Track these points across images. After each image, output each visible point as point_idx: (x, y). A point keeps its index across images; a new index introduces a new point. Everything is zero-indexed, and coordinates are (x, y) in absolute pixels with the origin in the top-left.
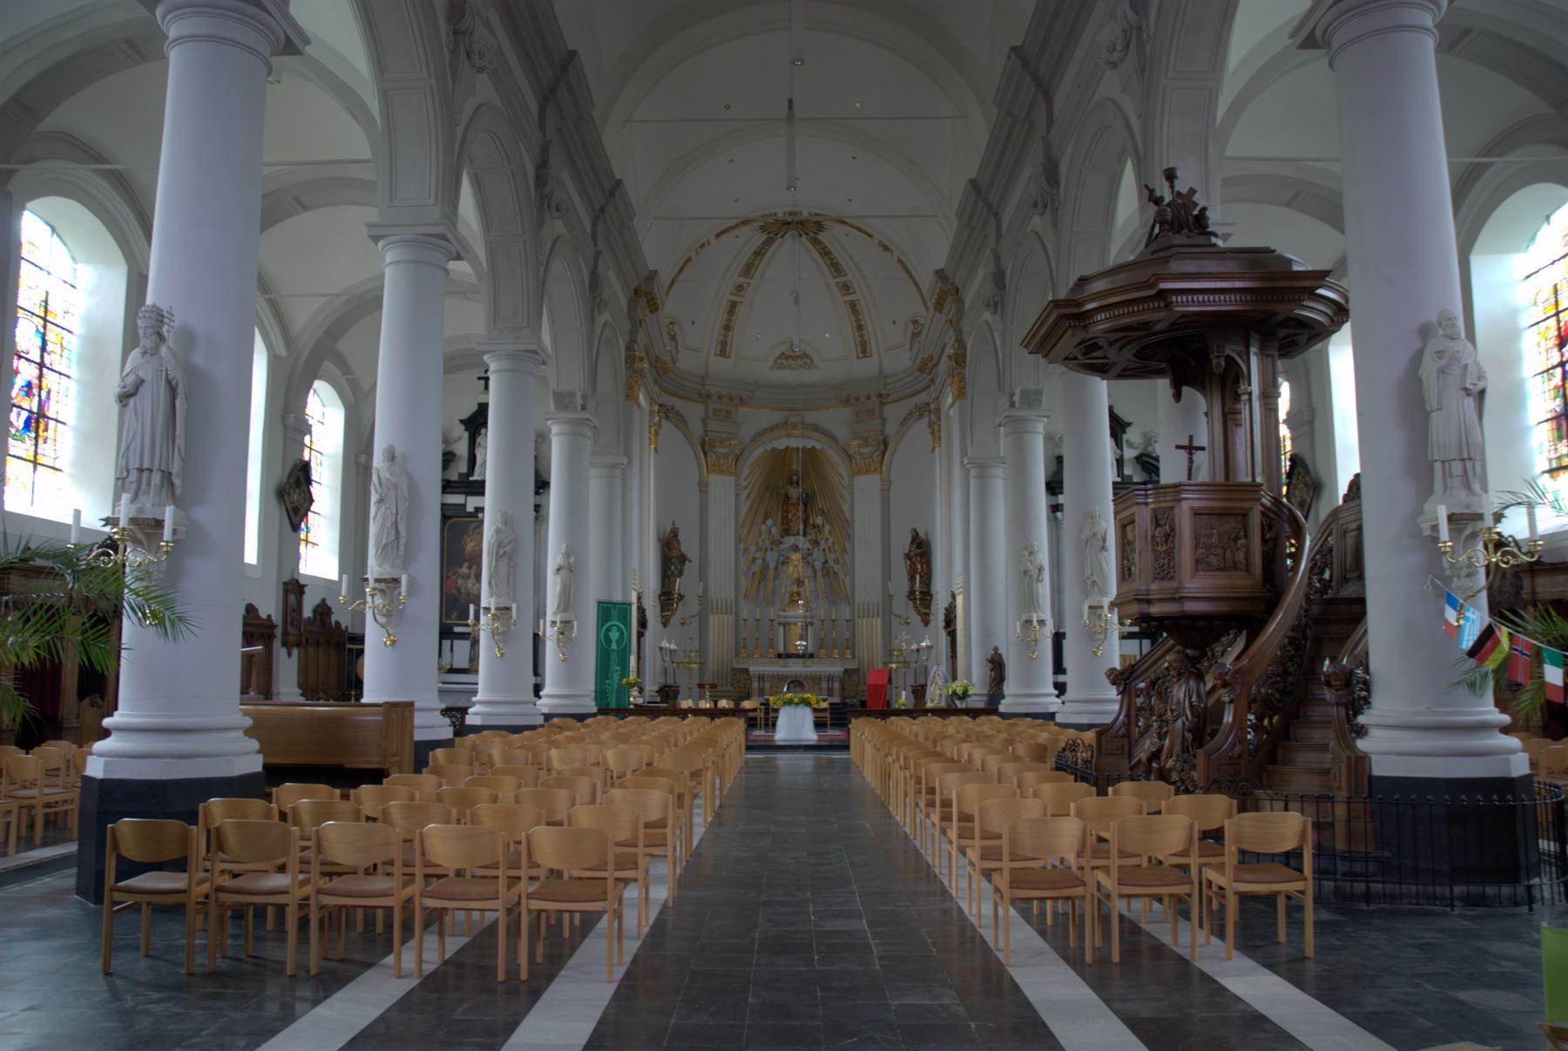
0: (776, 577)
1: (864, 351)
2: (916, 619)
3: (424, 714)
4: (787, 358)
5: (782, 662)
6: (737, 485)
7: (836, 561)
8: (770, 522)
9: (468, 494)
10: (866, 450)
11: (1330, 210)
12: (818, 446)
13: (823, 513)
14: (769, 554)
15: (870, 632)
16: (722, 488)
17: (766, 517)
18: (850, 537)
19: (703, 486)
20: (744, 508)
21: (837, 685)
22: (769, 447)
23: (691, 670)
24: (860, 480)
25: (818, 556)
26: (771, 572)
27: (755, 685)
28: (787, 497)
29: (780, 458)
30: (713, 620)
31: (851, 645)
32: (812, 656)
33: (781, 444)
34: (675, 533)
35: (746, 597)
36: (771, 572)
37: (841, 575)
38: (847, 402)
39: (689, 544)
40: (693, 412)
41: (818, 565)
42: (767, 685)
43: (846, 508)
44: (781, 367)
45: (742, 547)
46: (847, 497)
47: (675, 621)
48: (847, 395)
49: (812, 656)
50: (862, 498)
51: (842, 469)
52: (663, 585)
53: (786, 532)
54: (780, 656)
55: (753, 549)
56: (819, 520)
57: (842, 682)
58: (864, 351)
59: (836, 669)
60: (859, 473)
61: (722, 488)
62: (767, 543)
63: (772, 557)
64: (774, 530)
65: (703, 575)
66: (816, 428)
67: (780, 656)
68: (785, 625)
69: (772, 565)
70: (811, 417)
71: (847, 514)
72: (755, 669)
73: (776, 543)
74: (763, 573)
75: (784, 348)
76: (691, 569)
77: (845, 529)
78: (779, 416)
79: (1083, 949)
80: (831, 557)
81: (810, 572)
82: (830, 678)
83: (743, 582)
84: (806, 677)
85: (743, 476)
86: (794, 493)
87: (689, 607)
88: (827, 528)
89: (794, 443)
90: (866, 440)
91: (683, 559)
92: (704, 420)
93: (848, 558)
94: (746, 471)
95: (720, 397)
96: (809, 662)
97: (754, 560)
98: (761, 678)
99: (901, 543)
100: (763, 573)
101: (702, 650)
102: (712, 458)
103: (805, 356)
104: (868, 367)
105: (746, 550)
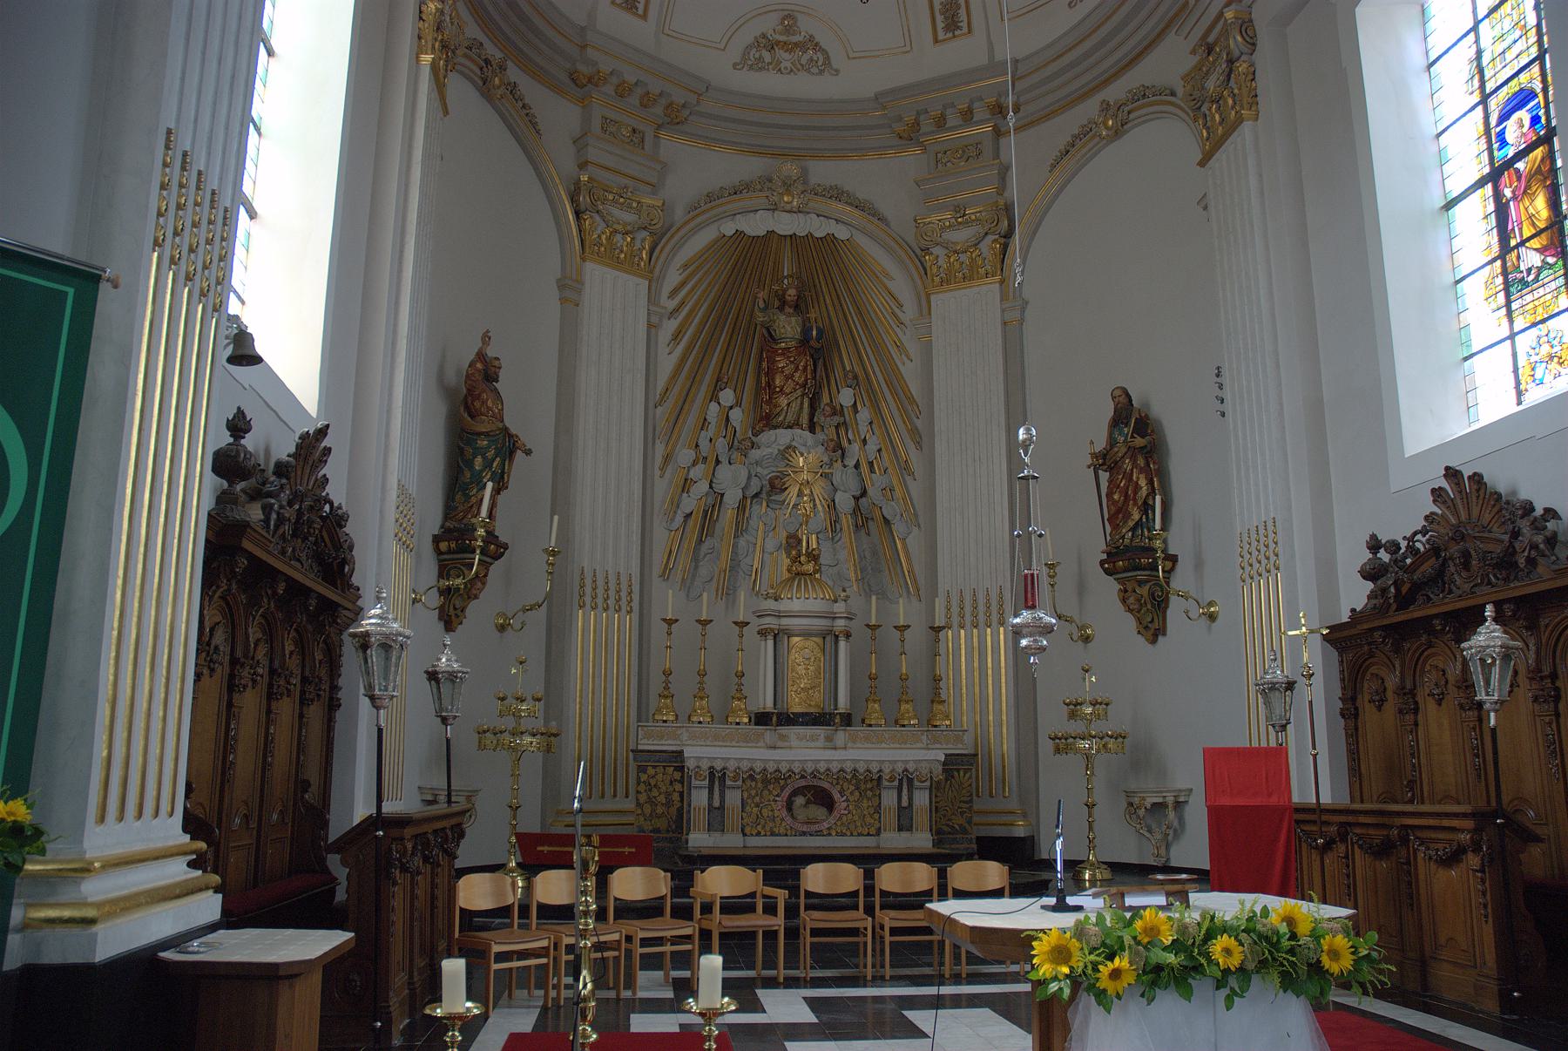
0: (740, 529)
1: (952, 25)
3: (159, 844)
4: (772, 46)
5: (768, 734)
6: (652, 300)
8: (727, 396)
9: (597, 875)
10: (961, 236)
12: (842, 233)
13: (855, 381)
14: (724, 472)
15: (981, 671)
16: (616, 303)
19: (570, 289)
20: (667, 363)
21: (922, 799)
22: (729, 229)
23: (518, 753)
24: (946, 303)
26: (728, 514)
27: (700, 798)
28: (771, 337)
29: (751, 255)
30: (585, 624)
31: (929, 698)
32: (847, 720)
33: (757, 225)
34: (485, 373)
35: (666, 574)
36: (728, 514)
37: (898, 528)
38: (910, 136)
39: (524, 405)
40: (559, 116)
41: (844, 501)
42: (733, 798)
43: (909, 371)
44: (759, 66)
45: (660, 450)
46: (912, 348)
47: (479, 613)
48: (909, 122)
49: (847, 720)
50: (951, 346)
51: (901, 285)
52: (449, 510)
53: (766, 420)
54: (762, 719)
55: (685, 456)
56: (846, 397)
57: (935, 788)
58: (952, 25)
59: (925, 755)
61: (616, 303)
62: (721, 444)
63: (732, 480)
64: (736, 416)
65: (561, 500)
66: (837, 194)
67: (762, 719)
68: (778, 635)
69: (732, 497)
70: (823, 172)
71: (915, 388)
72: (699, 753)
73: (740, 447)
74: (709, 516)
75: (769, 25)
76: (530, 473)
78: (750, 167)
80: (875, 484)
82: (906, 781)
83: (661, 537)
84: (840, 776)
85: (667, 287)
86: (788, 327)
87: (516, 582)
88: (864, 415)
89: (786, 224)
90: (959, 210)
91: (509, 446)
92: (580, 142)
93: (915, 488)
94: (673, 278)
95: (623, 91)
96: (841, 736)
97: (687, 485)
98: (717, 778)
100: (709, 516)
101: (552, 695)
102: (596, 227)
103: (812, 44)
104: (962, 54)
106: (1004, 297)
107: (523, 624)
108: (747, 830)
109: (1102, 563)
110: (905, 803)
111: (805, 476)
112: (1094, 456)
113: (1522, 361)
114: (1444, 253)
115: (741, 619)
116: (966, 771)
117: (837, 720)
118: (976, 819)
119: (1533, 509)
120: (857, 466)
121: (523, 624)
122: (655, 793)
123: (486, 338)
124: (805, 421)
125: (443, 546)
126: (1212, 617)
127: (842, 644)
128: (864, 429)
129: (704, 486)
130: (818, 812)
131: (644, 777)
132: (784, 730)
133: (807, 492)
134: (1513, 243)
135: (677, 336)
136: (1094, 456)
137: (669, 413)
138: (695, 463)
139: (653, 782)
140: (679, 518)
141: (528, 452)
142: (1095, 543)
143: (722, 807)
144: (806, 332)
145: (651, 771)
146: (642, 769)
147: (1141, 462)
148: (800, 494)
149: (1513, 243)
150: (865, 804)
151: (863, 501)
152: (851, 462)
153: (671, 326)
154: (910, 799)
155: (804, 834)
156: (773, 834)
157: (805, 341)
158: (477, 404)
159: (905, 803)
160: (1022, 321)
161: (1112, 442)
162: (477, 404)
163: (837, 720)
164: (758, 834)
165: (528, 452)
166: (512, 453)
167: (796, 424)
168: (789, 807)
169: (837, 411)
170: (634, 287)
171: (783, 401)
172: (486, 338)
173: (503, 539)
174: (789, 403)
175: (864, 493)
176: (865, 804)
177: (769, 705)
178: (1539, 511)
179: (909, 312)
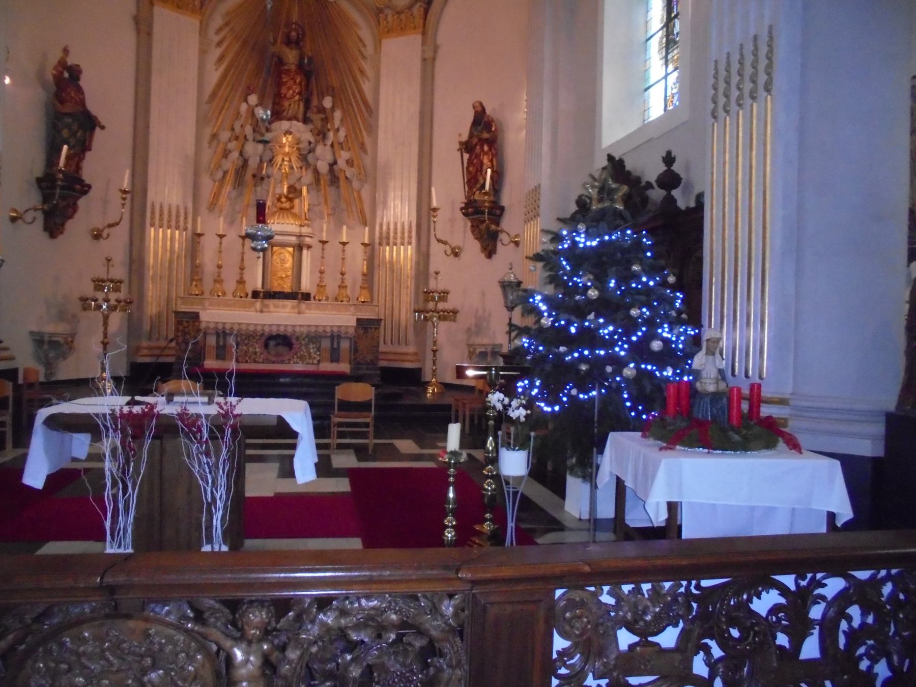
2: (472, 247)
7: (350, 163)
8: (253, 99)
11: (419, 361)
17: (249, 91)
18: (372, 129)
20: (214, 76)
25: (323, 156)
27: (212, 341)
37: (356, 184)
41: (323, 167)
43: (367, 87)
45: (208, 132)
51: (365, 33)
54: (255, 294)
55: (225, 135)
56: (328, 102)
60: (389, 32)
71: (369, 97)
77: (364, 114)
79: (279, 455)
81: (308, 177)
82: (335, 337)
86: (291, 56)
88: (338, 115)
93: (367, 160)
96: (303, 305)
97: (226, 154)
99: (453, 126)
105: (214, 136)
106: (424, 43)
107: (108, 235)
108: (240, 359)
109: (461, 209)
110: (335, 346)
111: (287, 149)
112: (461, 143)
113: (669, 93)
114: (642, 21)
115: (221, 233)
116: (376, 329)
117: (300, 296)
118: (381, 357)
119: (640, 182)
120: (332, 146)
121: (108, 235)
122: (188, 337)
123: (66, 51)
124: (300, 116)
125: (44, 184)
126: (517, 244)
127: (305, 252)
128: (337, 123)
129: (235, 155)
130: (282, 349)
131: (181, 328)
132: (267, 301)
133: (286, 159)
134: (673, 15)
135: (221, 58)
136: (461, 143)
137: (213, 104)
138: (230, 140)
139: (186, 330)
140: (219, 175)
141: (103, 128)
142: (460, 198)
143: (224, 346)
144: (301, 58)
145: (185, 324)
146: (179, 323)
147: (486, 148)
148: (283, 160)
149: (673, 15)
150: (311, 346)
151: (335, 167)
152: (329, 143)
153: (218, 52)
154: (339, 344)
155: (274, 362)
156: (255, 362)
157: (300, 66)
158: (64, 95)
159: (335, 346)
160: (434, 59)
161: (471, 136)
162: (64, 95)
163: (300, 296)
164: (247, 362)
165: (103, 128)
166: (92, 130)
167: (295, 118)
168: (266, 346)
169: (321, 110)
170: (189, 23)
171: (286, 104)
172: (66, 51)
173: (87, 182)
174: (294, 105)
175: (335, 163)
176: (311, 346)
177: (259, 286)
178: (643, 184)
179: (369, 50)
